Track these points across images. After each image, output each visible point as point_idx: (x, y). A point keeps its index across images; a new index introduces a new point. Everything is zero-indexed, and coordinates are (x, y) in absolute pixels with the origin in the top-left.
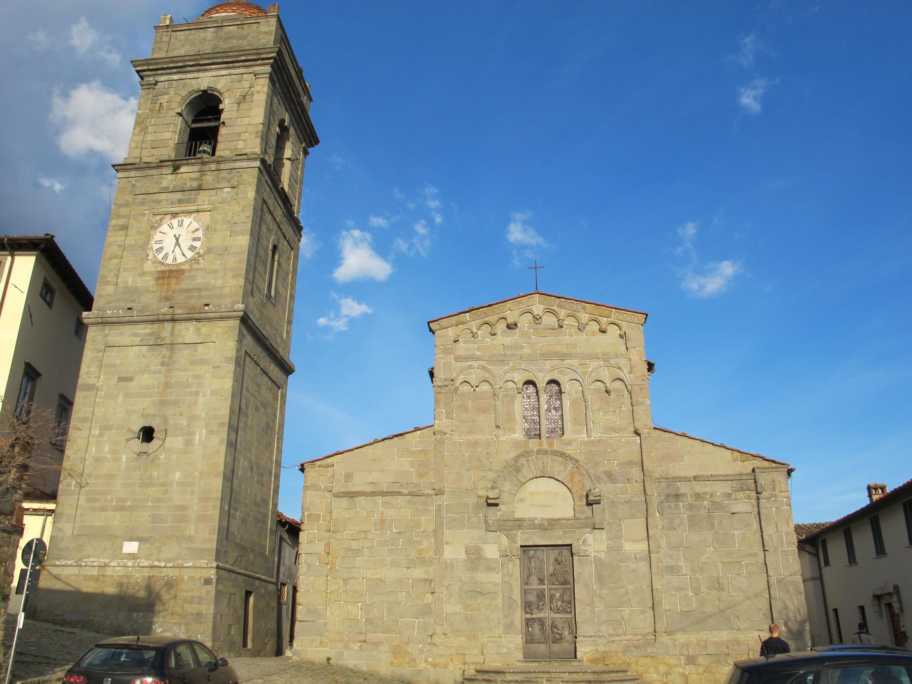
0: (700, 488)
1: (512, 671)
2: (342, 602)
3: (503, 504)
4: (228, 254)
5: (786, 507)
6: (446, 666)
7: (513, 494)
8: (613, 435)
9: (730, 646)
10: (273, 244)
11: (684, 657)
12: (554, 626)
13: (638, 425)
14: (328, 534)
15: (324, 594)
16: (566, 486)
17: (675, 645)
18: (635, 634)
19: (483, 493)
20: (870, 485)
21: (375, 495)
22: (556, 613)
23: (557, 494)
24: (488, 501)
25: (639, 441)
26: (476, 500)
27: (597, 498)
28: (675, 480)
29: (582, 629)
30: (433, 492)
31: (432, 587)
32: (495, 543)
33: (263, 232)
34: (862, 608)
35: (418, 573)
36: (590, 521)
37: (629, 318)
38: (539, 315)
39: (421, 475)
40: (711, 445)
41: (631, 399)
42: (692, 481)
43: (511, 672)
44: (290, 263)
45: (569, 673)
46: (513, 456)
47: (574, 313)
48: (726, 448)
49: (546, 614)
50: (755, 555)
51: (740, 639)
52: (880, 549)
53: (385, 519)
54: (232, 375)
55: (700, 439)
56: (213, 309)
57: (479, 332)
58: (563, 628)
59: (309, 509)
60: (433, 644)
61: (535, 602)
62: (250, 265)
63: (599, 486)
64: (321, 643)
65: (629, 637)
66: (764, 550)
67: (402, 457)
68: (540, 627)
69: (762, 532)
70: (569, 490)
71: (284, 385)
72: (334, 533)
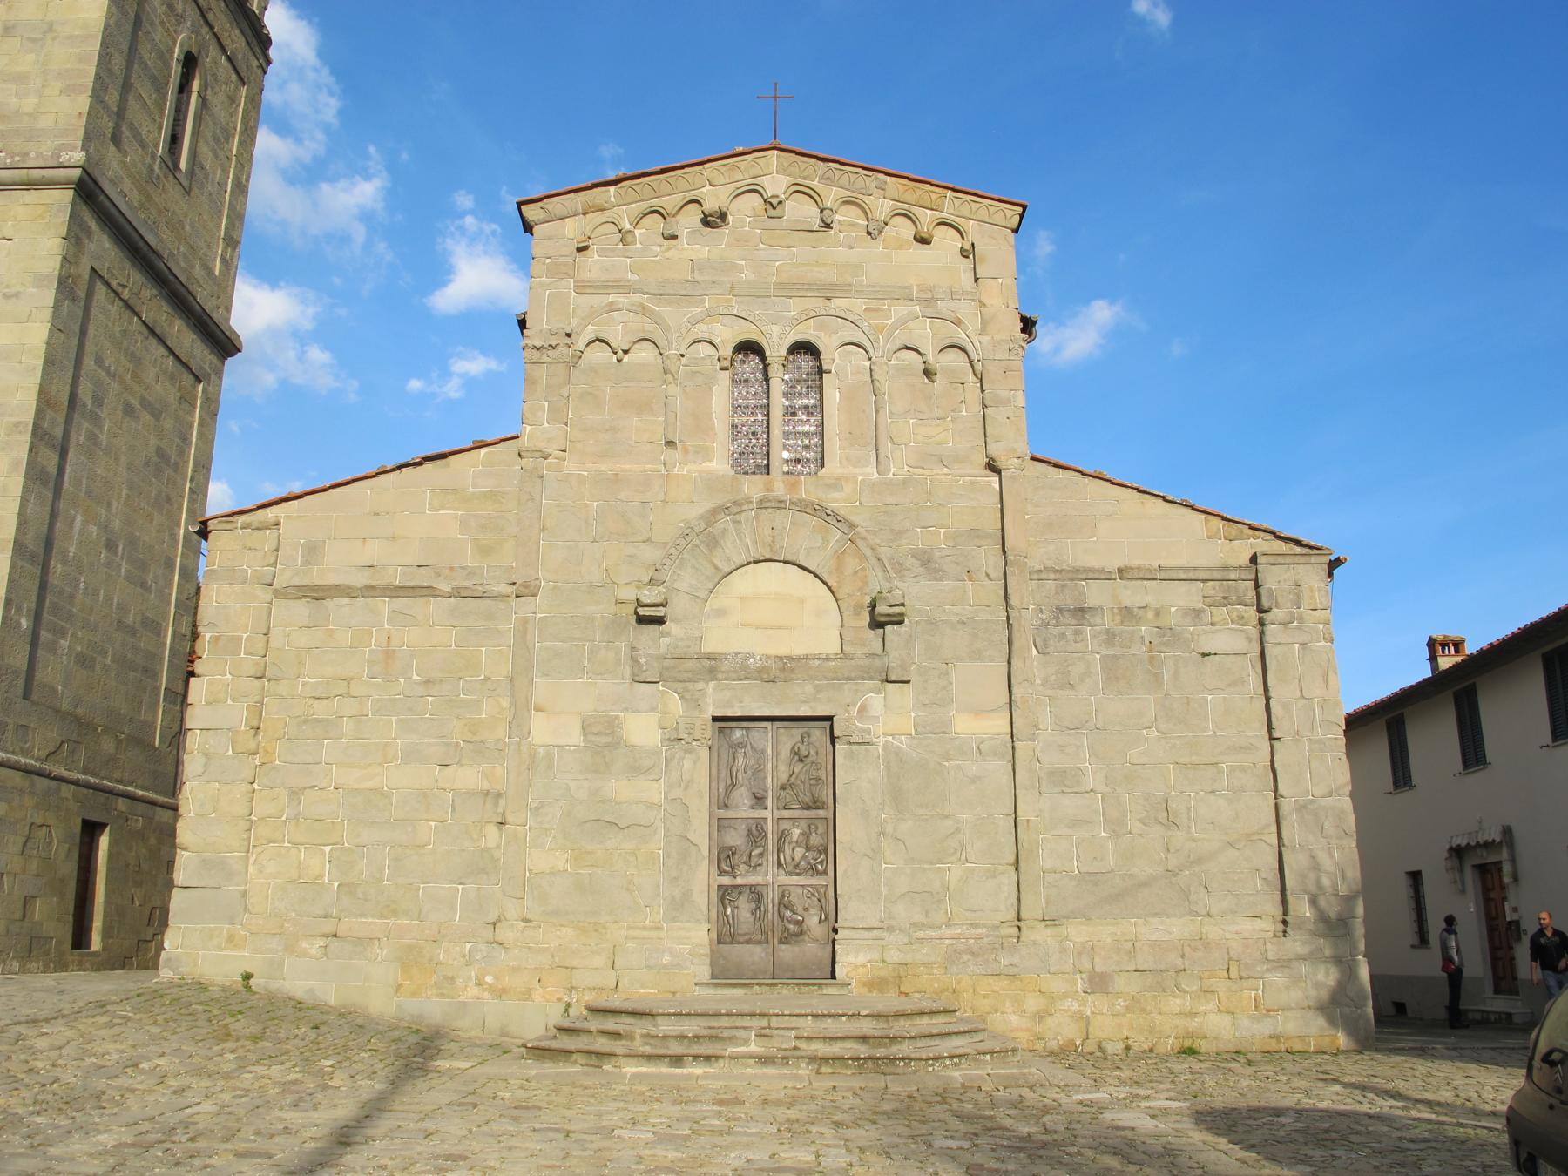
0: (1132, 594)
1: (672, 1011)
2: (286, 844)
3: (676, 621)
4: (54, 39)
5: (1323, 643)
6: (526, 995)
7: (699, 597)
8: (939, 471)
9: (1187, 950)
10: (186, 48)
11: (1084, 976)
12: (784, 903)
13: (996, 450)
14: (257, 683)
15: (243, 824)
16: (825, 583)
17: (1064, 950)
18: (972, 924)
19: (629, 594)
20: (1434, 636)
21: (371, 594)
22: (791, 874)
23: (802, 601)
24: (639, 610)
25: (997, 486)
26: (613, 609)
27: (897, 610)
28: (1075, 576)
29: (851, 911)
30: (511, 589)
31: (500, 810)
32: (653, 709)
33: (154, 10)
34: (1415, 877)
35: (469, 777)
36: (877, 663)
37: (983, 214)
38: (777, 196)
39: (485, 551)
40: (1160, 500)
41: (983, 391)
42: (1115, 579)
43: (669, 1015)
44: (236, 112)
45: (815, 1016)
46: (702, 511)
47: (860, 196)
48: (1194, 509)
49: (769, 876)
50: (1249, 749)
51: (1211, 937)
52: (1473, 753)
53: (394, 651)
54: (47, 314)
55: (1135, 485)
56: (8, 161)
57: (637, 232)
58: (806, 909)
59: (216, 625)
60: (497, 943)
61: (743, 847)
62: (110, 71)
63: (900, 584)
64: (231, 939)
65: (959, 931)
66: (1272, 739)
67: (442, 508)
68: (753, 905)
69: (1268, 699)
70: (832, 592)
72: (271, 682)
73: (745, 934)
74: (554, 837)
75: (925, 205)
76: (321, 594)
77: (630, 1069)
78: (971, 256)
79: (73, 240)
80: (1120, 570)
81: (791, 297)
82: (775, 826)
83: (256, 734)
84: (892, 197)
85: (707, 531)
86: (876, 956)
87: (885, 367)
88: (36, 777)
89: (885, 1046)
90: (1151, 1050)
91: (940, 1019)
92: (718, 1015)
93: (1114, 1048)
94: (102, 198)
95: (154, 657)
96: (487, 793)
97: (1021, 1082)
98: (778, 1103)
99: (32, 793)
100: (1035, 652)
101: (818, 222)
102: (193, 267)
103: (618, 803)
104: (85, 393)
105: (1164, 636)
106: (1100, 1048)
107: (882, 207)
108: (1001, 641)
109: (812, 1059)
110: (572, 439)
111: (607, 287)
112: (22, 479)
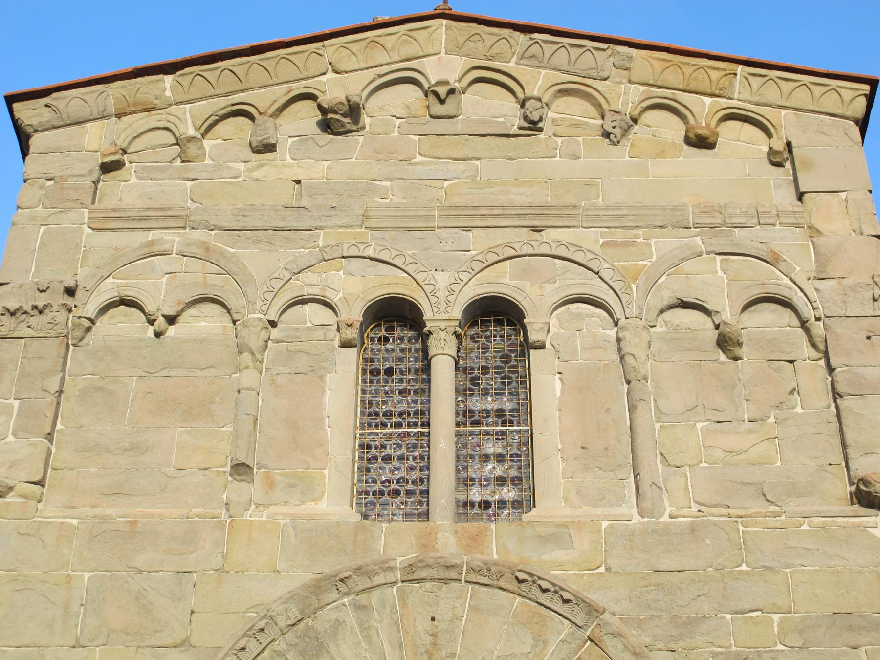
38: (446, 83)
41: (831, 369)
46: (294, 585)
75: (701, 89)
78: (788, 165)
81: (468, 229)
84: (643, 80)
85: (301, 626)
101: (518, 121)
110: (57, 465)
111: (148, 218)
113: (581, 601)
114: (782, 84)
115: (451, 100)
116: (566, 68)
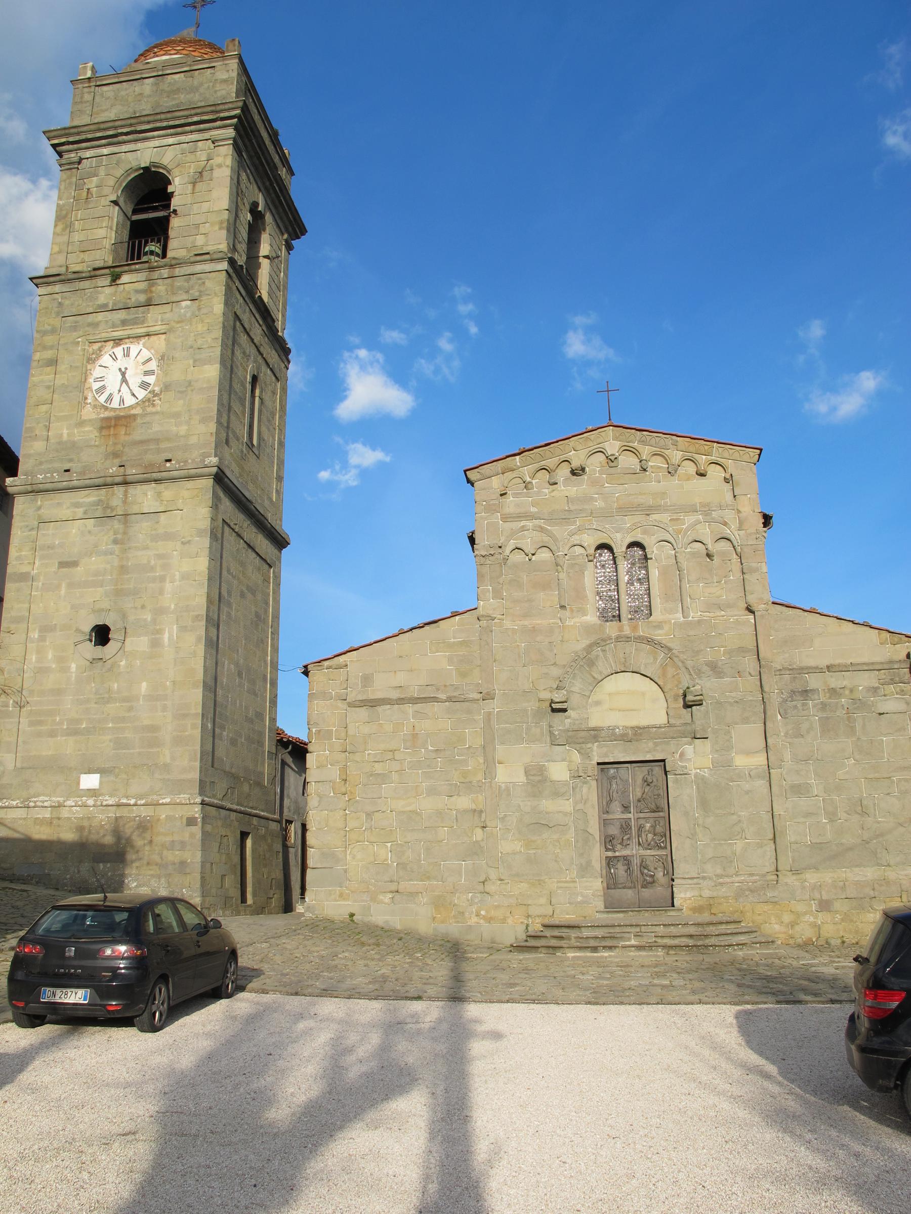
0: (835, 681)
1: (589, 925)
2: (366, 843)
3: (573, 709)
6: (504, 920)
8: (718, 614)
9: (876, 886)
10: (252, 374)
12: (643, 866)
13: (752, 599)
14: (343, 755)
17: (804, 888)
19: (546, 695)
22: (647, 849)
23: (643, 694)
24: (553, 705)
25: (753, 621)
26: (537, 704)
27: (698, 698)
29: (681, 869)
30: (480, 696)
32: (564, 760)
35: (464, 802)
36: (689, 728)
37: (736, 456)
38: (614, 455)
39: (463, 675)
41: (742, 564)
44: (276, 399)
46: (584, 646)
47: (663, 450)
49: (633, 851)
54: (207, 552)
55: (835, 615)
56: (177, 466)
57: (534, 482)
58: (656, 869)
59: (318, 724)
63: (699, 682)
64: (341, 895)
65: (743, 878)
67: (438, 652)
68: (626, 867)
70: (661, 688)
71: (277, 562)
73: (622, 883)
74: (513, 833)
76: (374, 704)
77: (571, 954)
78: (731, 482)
79: (214, 507)
80: (828, 667)
82: (636, 823)
83: (345, 783)
86: (697, 893)
87: (684, 554)
88: (221, 810)
89: (702, 940)
90: (857, 943)
91: (732, 926)
92: (614, 926)
93: (836, 942)
94: (226, 479)
95: (261, 734)
96: (475, 811)
97: (774, 956)
98: (649, 966)
99: (220, 819)
100: (779, 717)
101: (639, 467)
102: (264, 501)
103: (547, 813)
104: (225, 593)
105: (856, 704)
106: (827, 943)
107: (676, 456)
108: (760, 711)
109: (664, 947)
112: (204, 647)
113: (666, 647)
114: (730, 450)
115: (615, 461)
116: (655, 445)
